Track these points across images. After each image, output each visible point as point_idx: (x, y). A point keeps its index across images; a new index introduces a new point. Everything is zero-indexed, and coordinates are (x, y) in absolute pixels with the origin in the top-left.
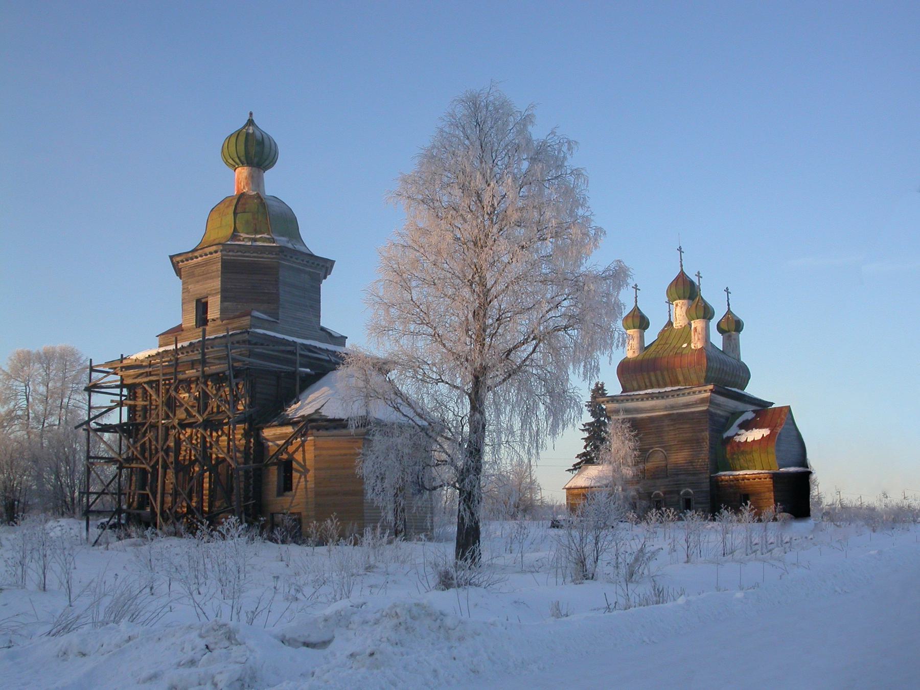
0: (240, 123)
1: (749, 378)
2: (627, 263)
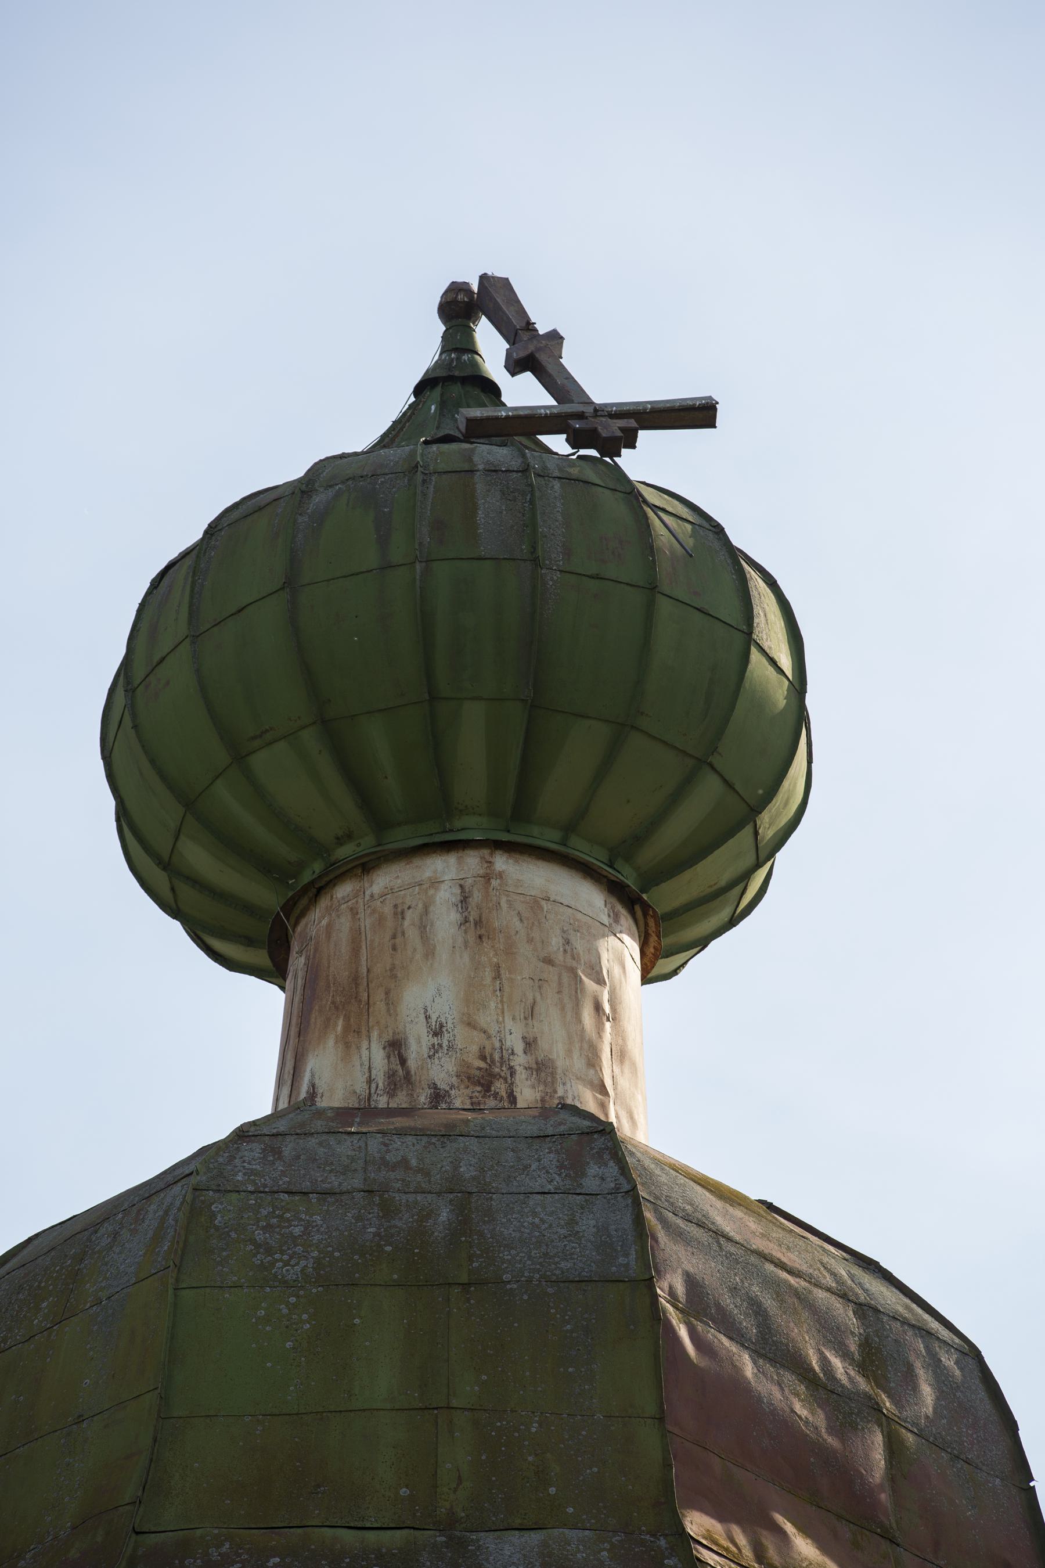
1: (505, 367)
2: (717, 428)
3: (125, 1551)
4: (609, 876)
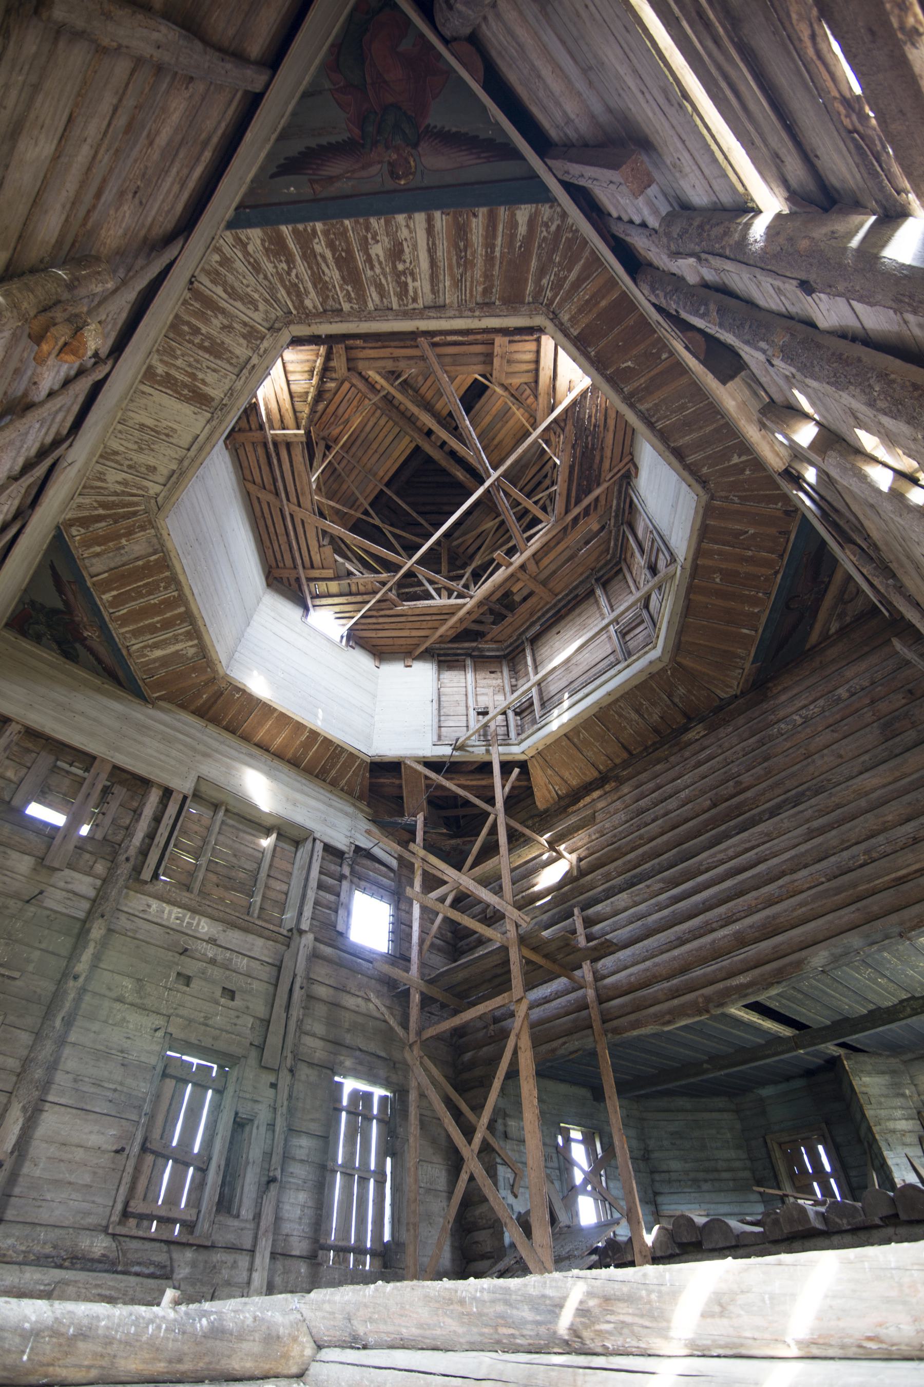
0: (9, 635)
3: (884, 786)
4: (283, 539)
